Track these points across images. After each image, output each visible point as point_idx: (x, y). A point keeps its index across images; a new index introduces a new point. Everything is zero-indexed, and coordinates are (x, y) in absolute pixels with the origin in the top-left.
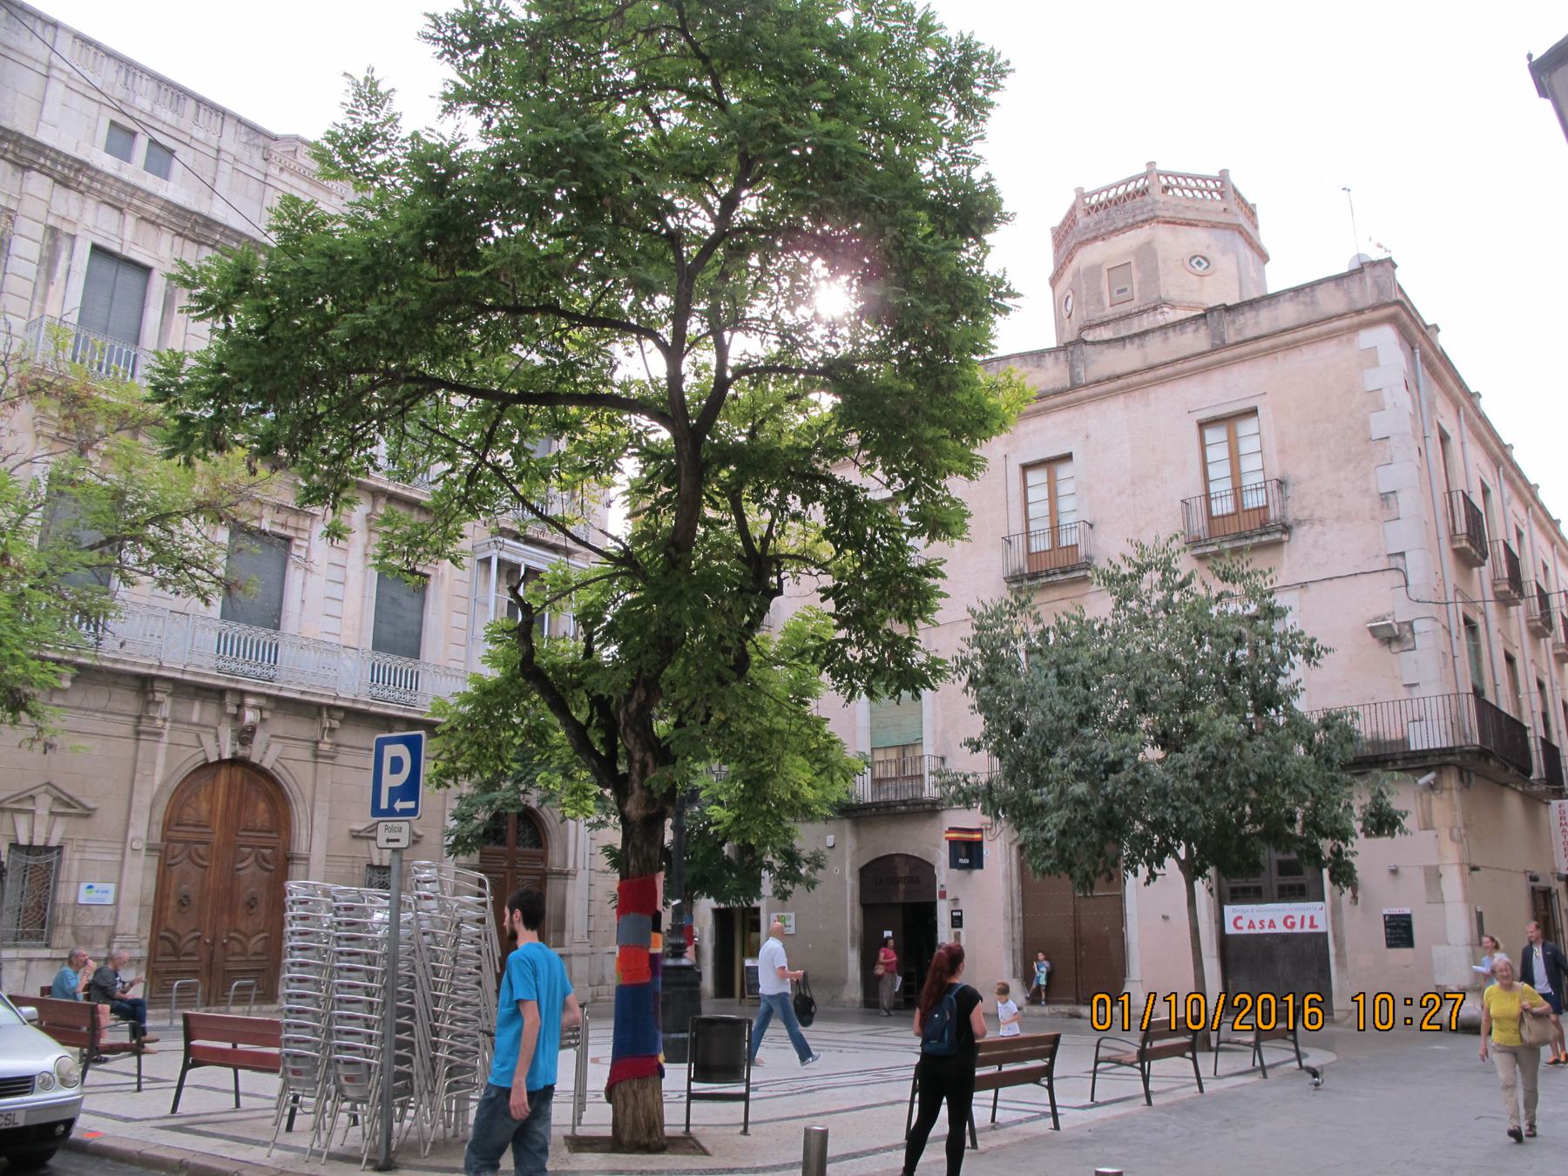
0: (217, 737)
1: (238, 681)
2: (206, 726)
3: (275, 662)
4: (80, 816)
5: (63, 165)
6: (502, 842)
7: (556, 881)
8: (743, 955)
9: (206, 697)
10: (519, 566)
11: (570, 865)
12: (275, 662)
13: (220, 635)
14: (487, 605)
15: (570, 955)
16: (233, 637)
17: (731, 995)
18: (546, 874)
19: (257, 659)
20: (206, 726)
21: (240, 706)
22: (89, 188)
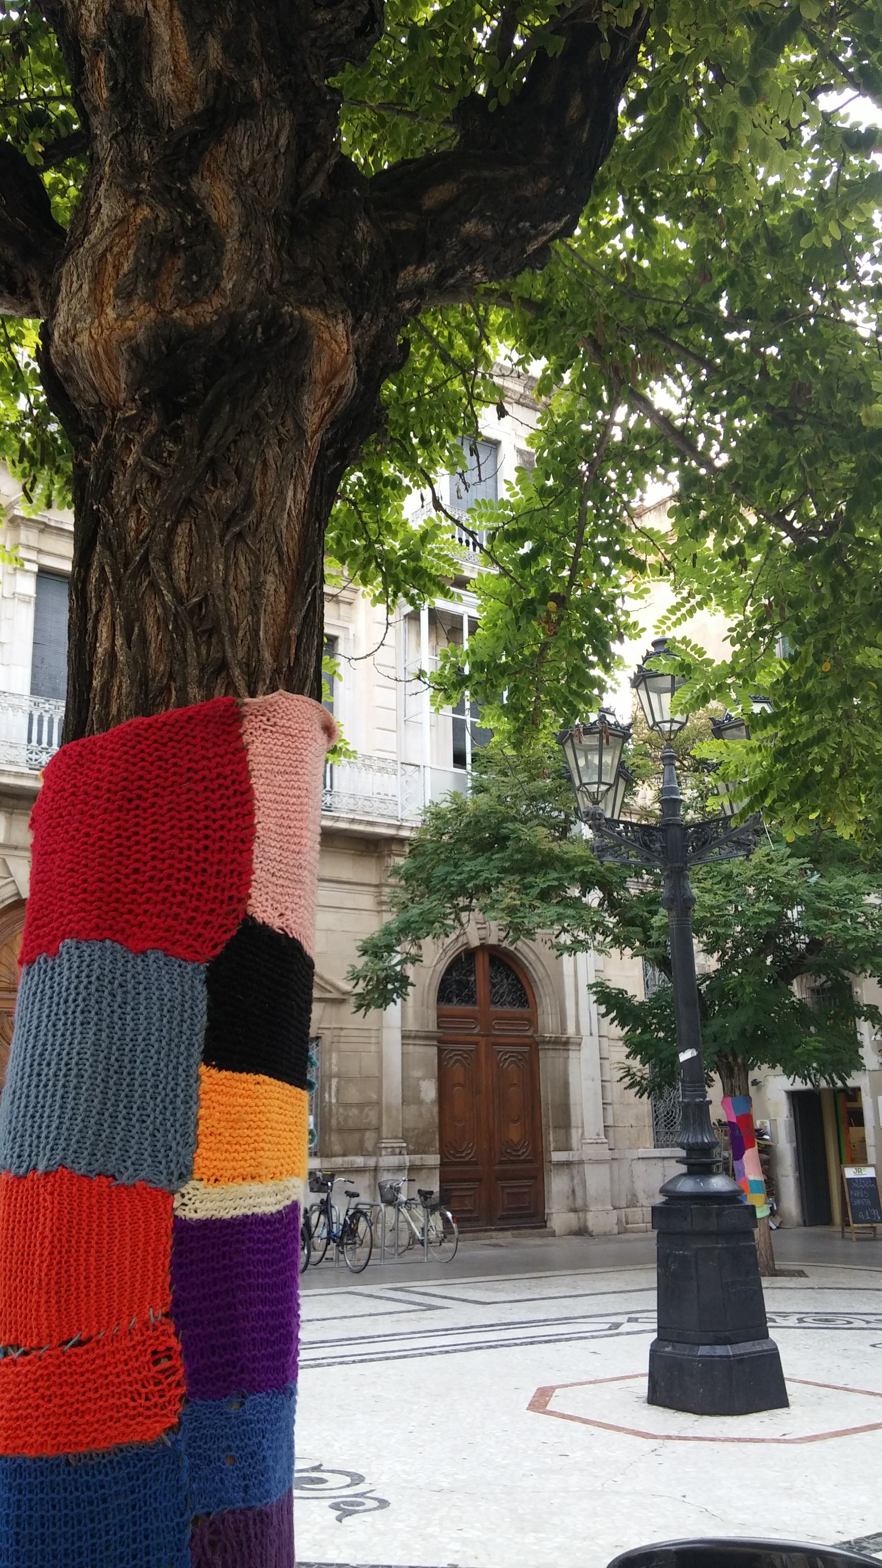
2: (16, 848)
3: (331, 787)
4: (333, 1001)
6: (470, 998)
7: (551, 1053)
8: (840, 1162)
10: (461, 618)
11: (571, 1030)
12: (331, 787)
15: (581, 1162)
17: (828, 1221)
18: (537, 1044)
20: (16, 848)
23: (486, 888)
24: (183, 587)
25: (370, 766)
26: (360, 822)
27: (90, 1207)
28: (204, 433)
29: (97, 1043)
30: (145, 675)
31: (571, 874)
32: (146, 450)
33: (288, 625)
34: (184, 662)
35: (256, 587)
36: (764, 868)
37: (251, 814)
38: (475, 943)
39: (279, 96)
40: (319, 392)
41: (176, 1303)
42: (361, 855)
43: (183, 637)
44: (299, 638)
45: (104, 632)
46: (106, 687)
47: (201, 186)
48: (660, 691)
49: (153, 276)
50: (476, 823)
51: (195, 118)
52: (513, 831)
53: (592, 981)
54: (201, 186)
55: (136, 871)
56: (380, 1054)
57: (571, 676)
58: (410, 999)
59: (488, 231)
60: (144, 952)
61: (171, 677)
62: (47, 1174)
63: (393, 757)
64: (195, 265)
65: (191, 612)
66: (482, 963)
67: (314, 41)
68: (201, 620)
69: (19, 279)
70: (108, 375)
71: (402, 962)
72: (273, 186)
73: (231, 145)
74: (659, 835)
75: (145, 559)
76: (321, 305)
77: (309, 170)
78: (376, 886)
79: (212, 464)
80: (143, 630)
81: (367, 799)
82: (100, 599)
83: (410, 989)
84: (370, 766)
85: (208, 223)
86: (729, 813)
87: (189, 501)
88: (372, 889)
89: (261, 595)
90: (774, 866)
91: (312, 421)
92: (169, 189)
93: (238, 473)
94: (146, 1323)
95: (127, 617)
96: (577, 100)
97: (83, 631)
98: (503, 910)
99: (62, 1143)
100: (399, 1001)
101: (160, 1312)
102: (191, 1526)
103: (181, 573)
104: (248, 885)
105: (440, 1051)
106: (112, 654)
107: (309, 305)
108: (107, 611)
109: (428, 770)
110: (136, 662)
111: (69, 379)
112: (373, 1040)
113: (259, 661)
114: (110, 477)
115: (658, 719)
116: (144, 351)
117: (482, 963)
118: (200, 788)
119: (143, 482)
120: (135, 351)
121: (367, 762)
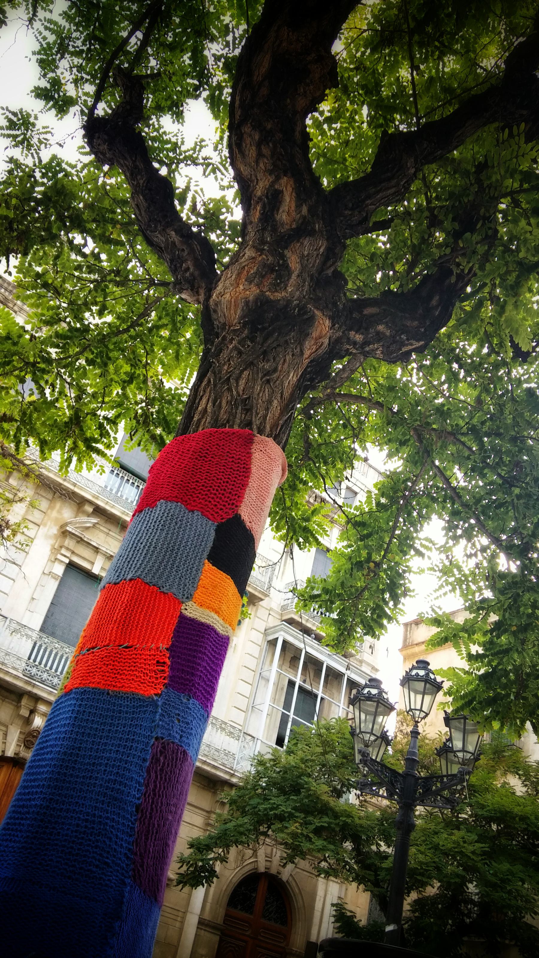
0: (5, 735)
1: (34, 686)
5: (6, 290)
9: (6, 697)
13: (35, 644)
14: (268, 680)
16: (41, 646)
19: (46, 666)
21: (32, 712)
22: (21, 309)
23: (281, 818)
24: (241, 393)
25: (224, 729)
26: (209, 764)
27: (147, 596)
28: (265, 339)
29: (166, 538)
30: (217, 418)
31: (337, 821)
32: (239, 343)
33: (279, 419)
34: (235, 417)
35: (270, 402)
36: (459, 845)
37: (248, 477)
38: (262, 869)
39: (325, 233)
40: (313, 342)
41: (173, 645)
42: (203, 789)
43: (237, 408)
44: (282, 426)
45: (204, 401)
46: (199, 421)
47: (288, 253)
48: (416, 692)
49: (263, 277)
50: (286, 770)
51: (292, 230)
52: (307, 783)
53: (335, 902)
54: (288, 253)
55: (197, 481)
56: (181, 929)
57: (374, 610)
58: (212, 889)
59: (388, 333)
60: (193, 511)
61: (228, 422)
62: (131, 580)
63: (240, 728)
64: (279, 277)
65: (242, 400)
66: (262, 887)
67: (341, 221)
68: (245, 405)
69: (196, 285)
70: (232, 312)
71: (215, 859)
72: (313, 266)
73: (302, 244)
74: (401, 779)
75: (228, 379)
76: (322, 310)
77: (328, 265)
78: (207, 812)
79: (265, 353)
80: (220, 403)
81: (217, 750)
82: (204, 391)
83: (215, 879)
84: (224, 729)
85: (287, 266)
86: (445, 773)
87: (252, 363)
88: (204, 813)
89: (271, 405)
90: (466, 845)
91: (307, 353)
92: (276, 250)
93: (274, 359)
94: (158, 648)
95: (215, 397)
96: (437, 298)
97: (195, 399)
98: (288, 834)
99: (141, 570)
100: (206, 885)
101: (165, 647)
102: (154, 740)
103: (241, 388)
104: (241, 502)
105: (220, 938)
106: (205, 410)
107: (318, 309)
108: (207, 394)
109: (259, 742)
110: (215, 412)
111: (215, 311)
112: (179, 919)
113: (264, 427)
114: (221, 351)
115: (413, 707)
116: (250, 304)
117: (262, 887)
118: (231, 460)
119: (234, 354)
120: (247, 303)
121: (223, 726)
